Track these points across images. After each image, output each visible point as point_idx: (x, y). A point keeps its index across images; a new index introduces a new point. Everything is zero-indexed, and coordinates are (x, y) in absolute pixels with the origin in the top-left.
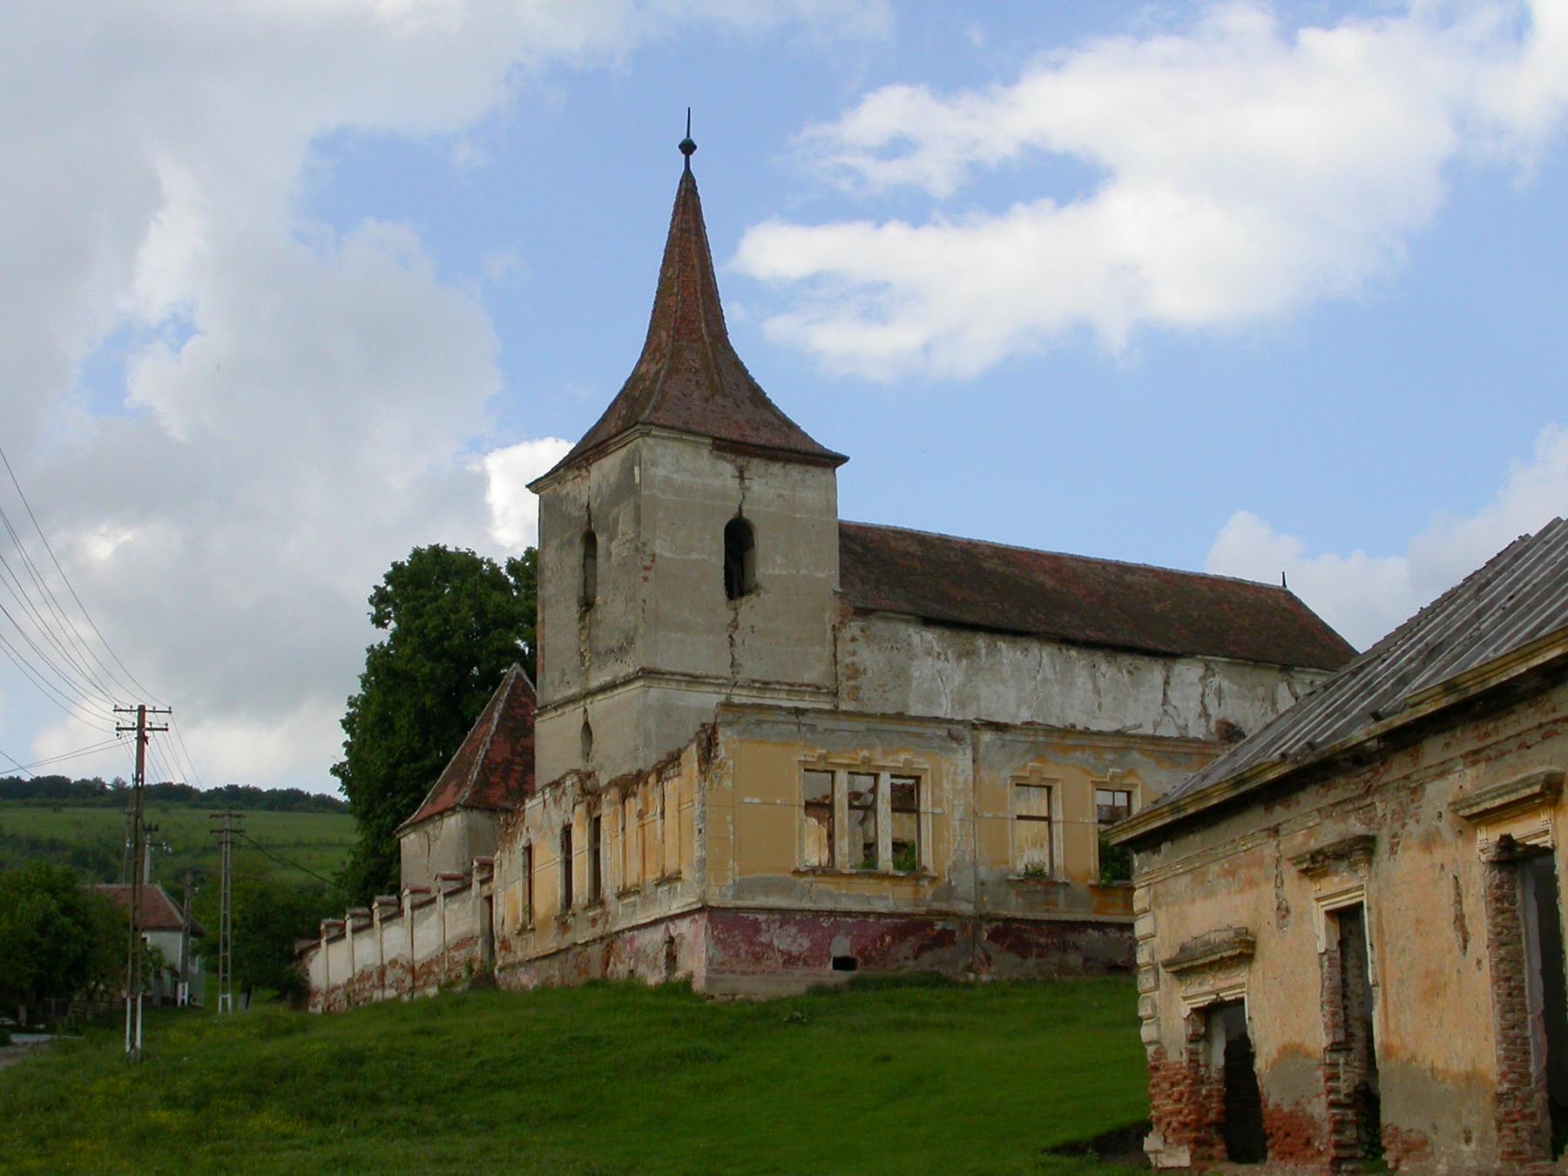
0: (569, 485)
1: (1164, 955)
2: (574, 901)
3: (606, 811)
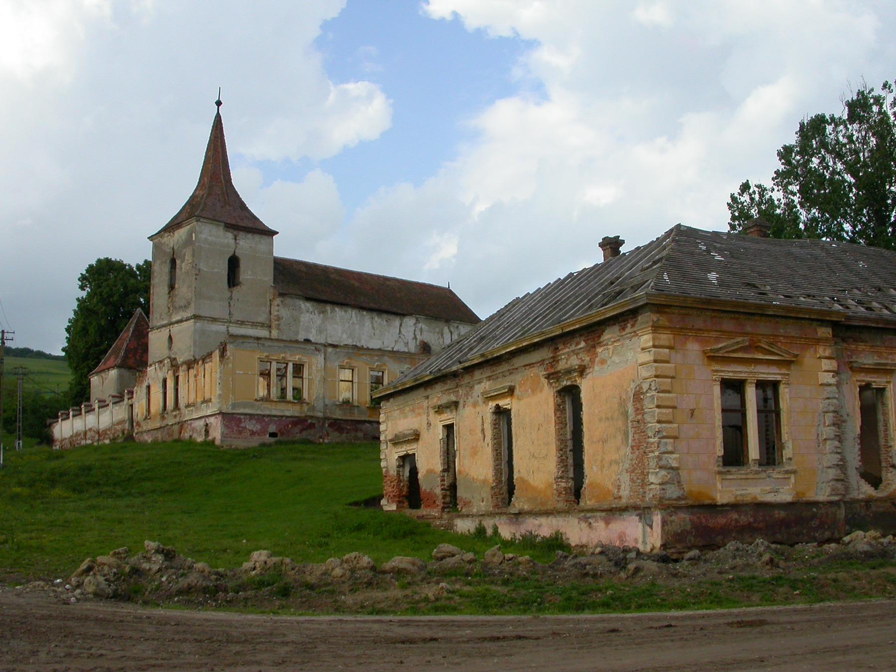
0: (165, 239)
1: (390, 437)
2: (167, 408)
3: (181, 374)
